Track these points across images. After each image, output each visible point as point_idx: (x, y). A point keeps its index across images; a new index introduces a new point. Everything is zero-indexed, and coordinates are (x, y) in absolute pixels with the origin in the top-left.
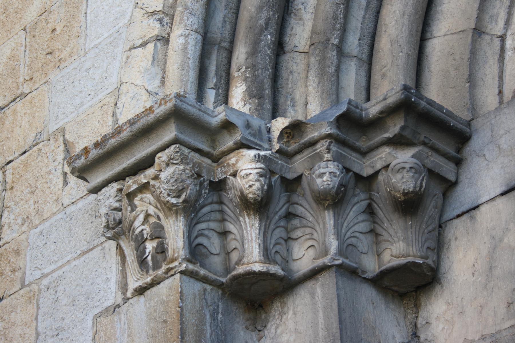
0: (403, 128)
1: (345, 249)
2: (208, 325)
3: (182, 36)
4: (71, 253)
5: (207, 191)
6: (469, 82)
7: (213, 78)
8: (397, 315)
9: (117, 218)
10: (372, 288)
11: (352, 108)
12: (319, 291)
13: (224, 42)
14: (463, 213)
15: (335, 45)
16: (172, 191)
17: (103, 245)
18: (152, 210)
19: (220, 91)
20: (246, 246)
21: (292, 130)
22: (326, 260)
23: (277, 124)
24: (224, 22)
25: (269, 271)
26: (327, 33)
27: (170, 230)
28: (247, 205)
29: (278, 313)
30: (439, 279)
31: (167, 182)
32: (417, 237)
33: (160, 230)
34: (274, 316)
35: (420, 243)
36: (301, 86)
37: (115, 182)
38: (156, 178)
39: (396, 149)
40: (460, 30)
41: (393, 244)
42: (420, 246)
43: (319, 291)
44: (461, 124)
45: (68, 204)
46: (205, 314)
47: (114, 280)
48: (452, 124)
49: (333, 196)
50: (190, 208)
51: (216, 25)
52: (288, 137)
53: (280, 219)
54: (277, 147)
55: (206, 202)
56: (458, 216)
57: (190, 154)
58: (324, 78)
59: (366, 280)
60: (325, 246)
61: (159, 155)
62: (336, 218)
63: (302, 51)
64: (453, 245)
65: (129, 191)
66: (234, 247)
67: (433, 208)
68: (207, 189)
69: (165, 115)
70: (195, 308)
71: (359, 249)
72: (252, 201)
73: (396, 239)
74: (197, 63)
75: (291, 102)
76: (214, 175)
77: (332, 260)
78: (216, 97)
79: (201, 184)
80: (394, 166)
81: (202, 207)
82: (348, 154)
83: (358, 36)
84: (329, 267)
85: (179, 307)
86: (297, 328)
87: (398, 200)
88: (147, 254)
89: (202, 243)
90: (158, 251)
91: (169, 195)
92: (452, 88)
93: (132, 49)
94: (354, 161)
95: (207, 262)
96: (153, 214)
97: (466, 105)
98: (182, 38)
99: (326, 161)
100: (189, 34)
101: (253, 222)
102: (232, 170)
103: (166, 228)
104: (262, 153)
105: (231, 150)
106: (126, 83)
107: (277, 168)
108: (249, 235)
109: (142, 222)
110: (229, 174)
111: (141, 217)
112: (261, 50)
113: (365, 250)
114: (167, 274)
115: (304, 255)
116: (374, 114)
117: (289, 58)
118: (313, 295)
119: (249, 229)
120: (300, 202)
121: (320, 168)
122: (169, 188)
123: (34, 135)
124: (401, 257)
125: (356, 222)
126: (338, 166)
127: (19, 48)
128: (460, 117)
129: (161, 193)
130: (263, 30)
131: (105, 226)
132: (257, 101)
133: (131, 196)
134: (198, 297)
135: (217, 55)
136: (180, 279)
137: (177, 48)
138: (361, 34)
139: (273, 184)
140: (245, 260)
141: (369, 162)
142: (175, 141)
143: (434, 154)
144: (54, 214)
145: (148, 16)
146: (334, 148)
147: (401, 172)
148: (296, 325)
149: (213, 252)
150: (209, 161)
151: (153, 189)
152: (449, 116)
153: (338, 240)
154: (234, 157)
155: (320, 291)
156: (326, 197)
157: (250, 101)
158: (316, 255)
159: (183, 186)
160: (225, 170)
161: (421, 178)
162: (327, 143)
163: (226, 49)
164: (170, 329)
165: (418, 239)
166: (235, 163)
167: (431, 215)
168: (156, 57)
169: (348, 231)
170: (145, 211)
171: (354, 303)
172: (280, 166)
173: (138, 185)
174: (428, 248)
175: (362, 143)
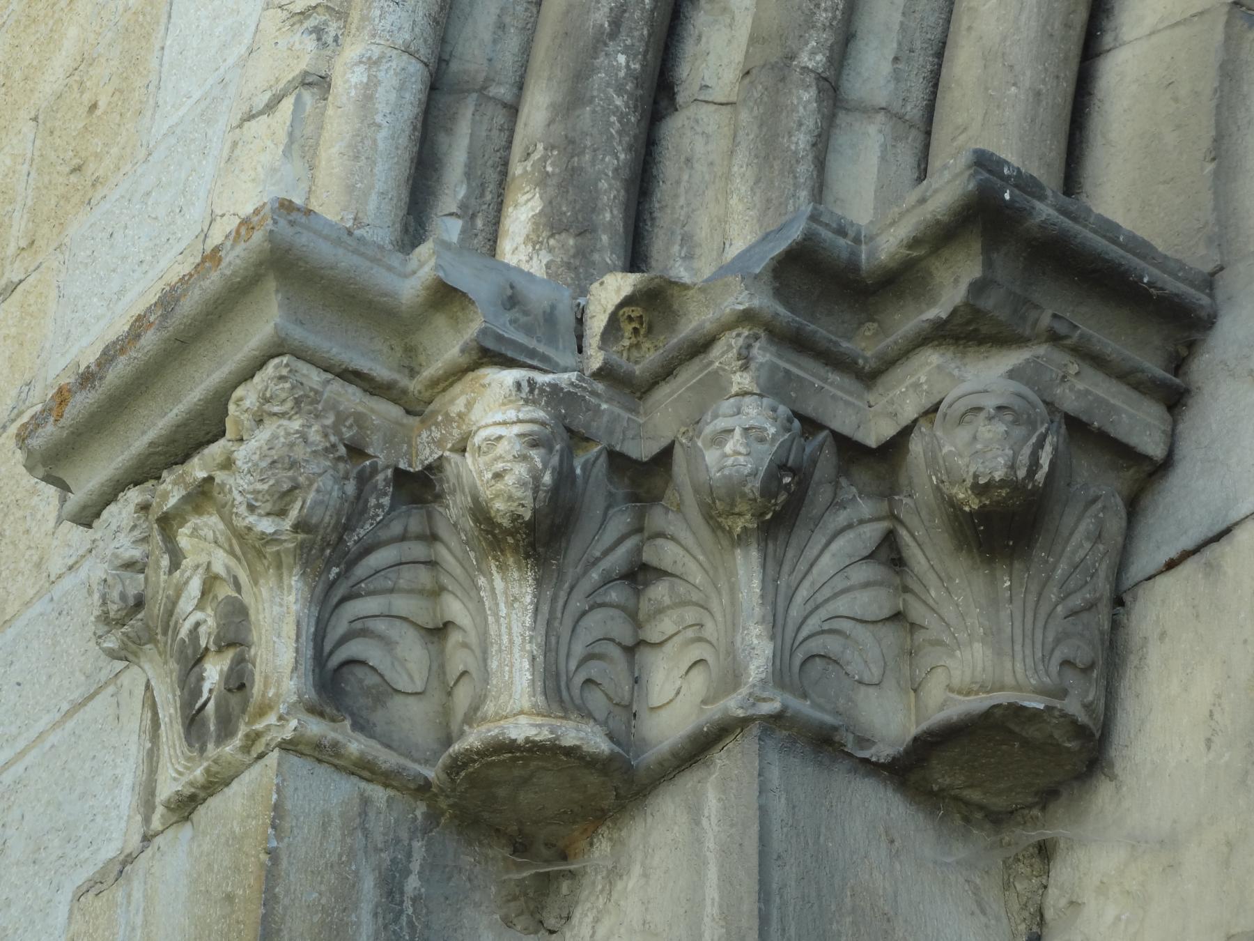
0: (978, 288)
1: (796, 668)
2: (366, 910)
3: (361, 62)
4: (48, 711)
5: (386, 501)
6: (1214, 159)
7: (456, 186)
8: (978, 881)
9: (132, 592)
10: (890, 793)
11: (826, 234)
12: (712, 802)
13: (500, 84)
14: (1186, 555)
15: (812, 71)
16: (260, 497)
17: (119, 682)
19: (479, 223)
20: (494, 665)
21: (645, 309)
22: (733, 705)
23: (603, 294)
24: (501, 26)
25: (557, 738)
26: (787, 38)
27: (261, 617)
28: (494, 536)
29: (604, 873)
30: (1111, 765)
31: (249, 472)
32: (1029, 626)
33: (239, 620)
34: (594, 883)
35: (1038, 646)
36: (717, 199)
37: (135, 486)
38: (228, 464)
39: (964, 354)
40: (1194, 11)
41: (954, 651)
43: (712, 802)
44: (1183, 280)
45: (59, 572)
46: (357, 876)
47: (128, 781)
48: (1145, 280)
49: (755, 500)
50: (322, 550)
51: (476, 37)
52: (636, 331)
53: (607, 581)
54: (596, 359)
55: (384, 534)
56: (1171, 565)
57: (329, 388)
58: (772, 167)
59: (871, 768)
60: (734, 659)
61: (239, 392)
62: (771, 571)
63: (723, 100)
64: (1154, 655)
65: (165, 509)
66: (461, 668)
67: (1088, 538)
68: (385, 494)
69: (246, 269)
70: (322, 856)
71: (849, 669)
72: (506, 523)
73: (962, 636)
74: (403, 141)
75: (682, 246)
76: (408, 453)
79: (363, 479)
80: (950, 406)
81: (367, 551)
82: (813, 375)
83: (890, 50)
84: (744, 723)
85: (268, 853)
86: (649, 918)
87: (961, 509)
88: (205, 695)
89: (362, 657)
92: (1165, 182)
93: (245, 120)
94: (834, 397)
95: (378, 717)
97: (1204, 227)
98: (362, 68)
99: (737, 395)
100: (380, 58)
101: (516, 591)
103: (252, 612)
104: (541, 378)
105: (457, 374)
106: (223, 216)
107: (594, 424)
108: (503, 629)
109: (196, 601)
110: (449, 446)
111: (195, 587)
112: (593, 97)
113: (875, 673)
114: (249, 752)
115: (678, 693)
116: (893, 249)
117: (686, 123)
118: (695, 812)
119: (503, 611)
120: (671, 530)
121: (715, 416)
122: (251, 488)
123: (14, 393)
124: (977, 693)
125: (839, 587)
126: (774, 410)
127: (18, 167)
128: (1177, 261)
130: (600, 42)
131: (98, 617)
132: (571, 242)
133: (167, 523)
134: (337, 821)
135: (473, 122)
136: (279, 764)
137: (344, 99)
138: (900, 44)
139: (578, 471)
140: (489, 708)
141: (883, 401)
142: (276, 349)
143: (1089, 371)
144: (27, 604)
145: (292, 26)
146: (762, 354)
147: (970, 423)
148: (647, 909)
149: (400, 687)
150: (395, 411)
152: (1135, 254)
153: (773, 637)
154: (462, 392)
155: (714, 801)
156: (733, 505)
157: (552, 242)
158: (708, 689)
159: (293, 479)
160: (438, 435)
161: (1034, 440)
162: (741, 341)
163: (505, 105)
164: (238, 922)
165: (1033, 635)
166: (463, 410)
167: (1077, 560)
168: (297, 133)
169: (811, 613)
170: (205, 565)
171: (822, 839)
172: (605, 419)
173: (186, 489)
174: (1066, 663)
175: (863, 345)
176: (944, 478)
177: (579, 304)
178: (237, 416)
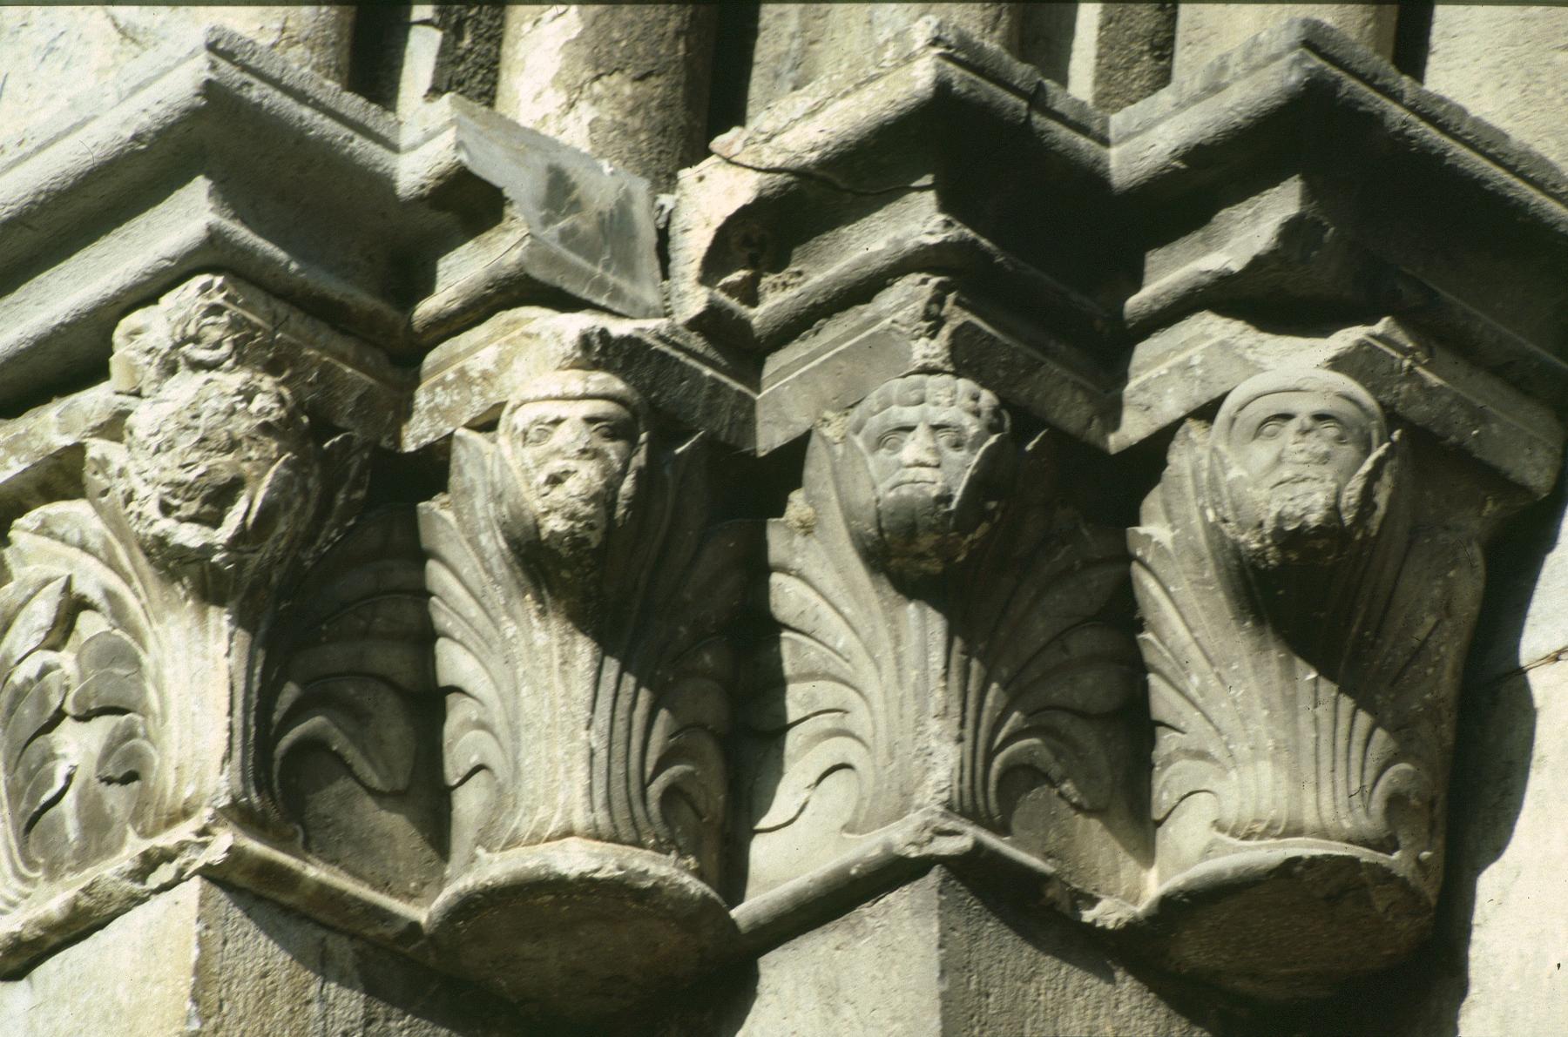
16: (180, 492)
18: (92, 579)
22: (900, 836)
38: (114, 427)
41: (1225, 770)
42: (1355, 785)
54: (693, 300)
66: (474, 760)
73: (1241, 749)
77: (927, 834)
78: (440, 67)
90: (110, 771)
91: (166, 509)
96: (95, 595)
102: (477, 406)
109: (42, 635)
110: (465, 420)
111: (43, 611)
114: (144, 882)
122: (167, 477)
124: (1262, 836)
129: (129, 498)
132: (627, 89)
140: (522, 823)
147: (1273, 435)
151: (98, 477)
154: (489, 340)
161: (1367, 466)
170: (61, 583)
176: (1229, 514)
177: (662, 208)
178: (131, 359)
